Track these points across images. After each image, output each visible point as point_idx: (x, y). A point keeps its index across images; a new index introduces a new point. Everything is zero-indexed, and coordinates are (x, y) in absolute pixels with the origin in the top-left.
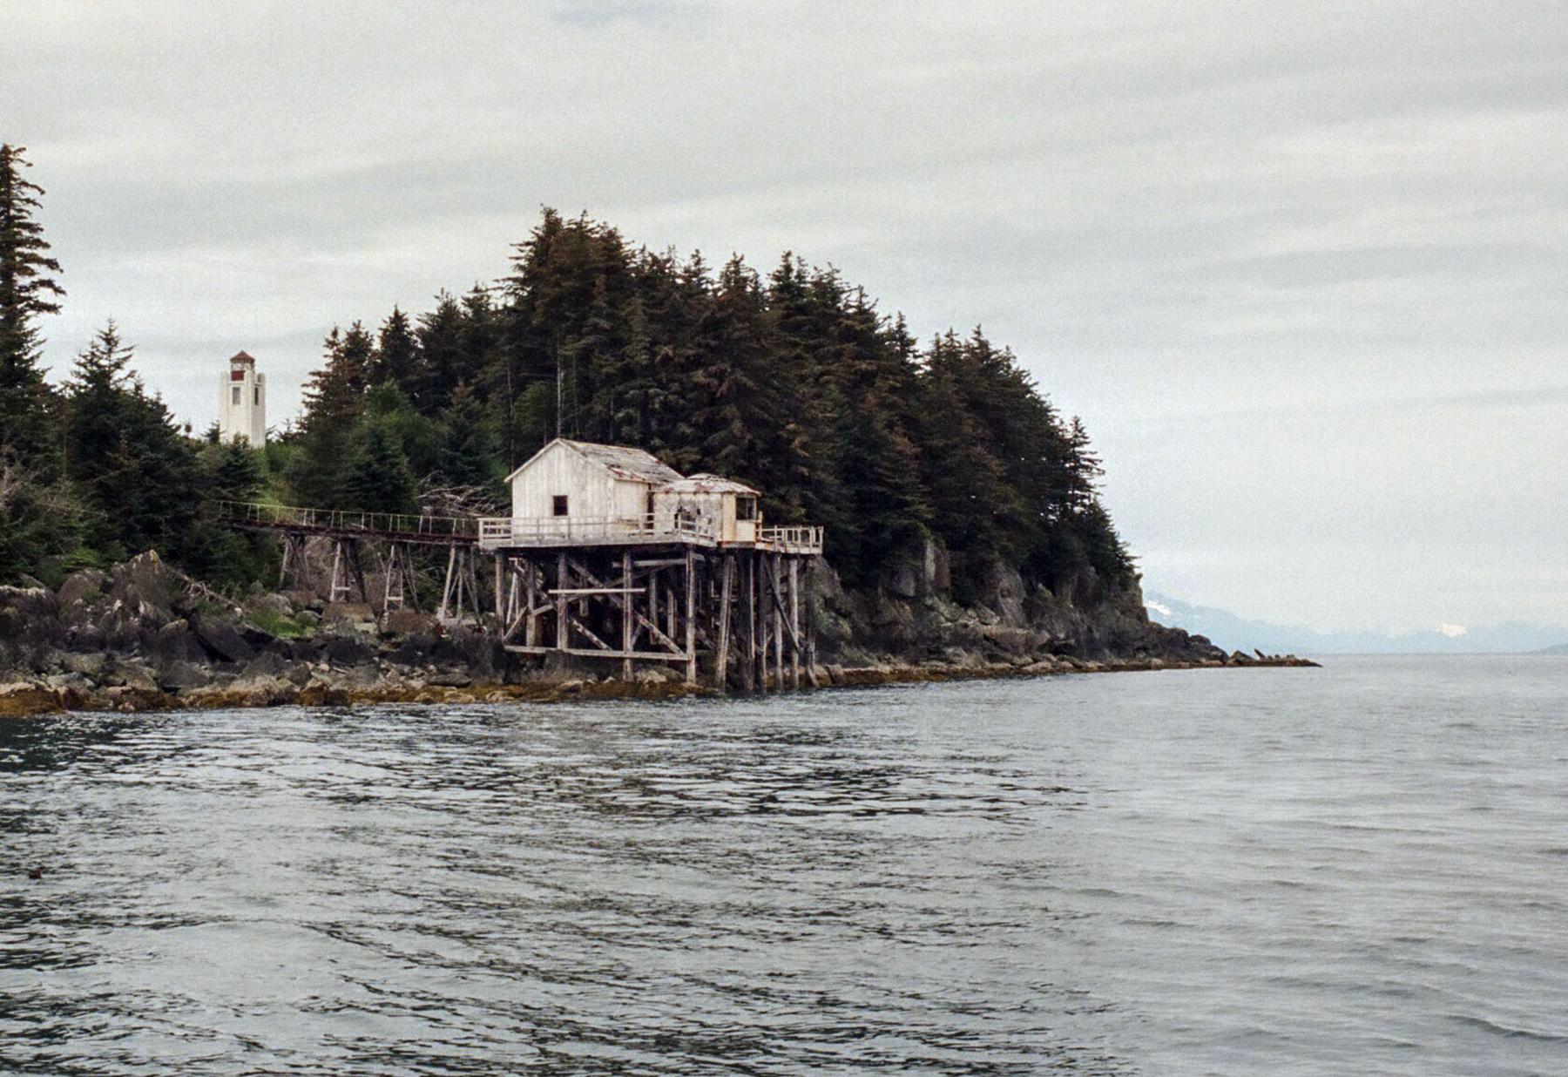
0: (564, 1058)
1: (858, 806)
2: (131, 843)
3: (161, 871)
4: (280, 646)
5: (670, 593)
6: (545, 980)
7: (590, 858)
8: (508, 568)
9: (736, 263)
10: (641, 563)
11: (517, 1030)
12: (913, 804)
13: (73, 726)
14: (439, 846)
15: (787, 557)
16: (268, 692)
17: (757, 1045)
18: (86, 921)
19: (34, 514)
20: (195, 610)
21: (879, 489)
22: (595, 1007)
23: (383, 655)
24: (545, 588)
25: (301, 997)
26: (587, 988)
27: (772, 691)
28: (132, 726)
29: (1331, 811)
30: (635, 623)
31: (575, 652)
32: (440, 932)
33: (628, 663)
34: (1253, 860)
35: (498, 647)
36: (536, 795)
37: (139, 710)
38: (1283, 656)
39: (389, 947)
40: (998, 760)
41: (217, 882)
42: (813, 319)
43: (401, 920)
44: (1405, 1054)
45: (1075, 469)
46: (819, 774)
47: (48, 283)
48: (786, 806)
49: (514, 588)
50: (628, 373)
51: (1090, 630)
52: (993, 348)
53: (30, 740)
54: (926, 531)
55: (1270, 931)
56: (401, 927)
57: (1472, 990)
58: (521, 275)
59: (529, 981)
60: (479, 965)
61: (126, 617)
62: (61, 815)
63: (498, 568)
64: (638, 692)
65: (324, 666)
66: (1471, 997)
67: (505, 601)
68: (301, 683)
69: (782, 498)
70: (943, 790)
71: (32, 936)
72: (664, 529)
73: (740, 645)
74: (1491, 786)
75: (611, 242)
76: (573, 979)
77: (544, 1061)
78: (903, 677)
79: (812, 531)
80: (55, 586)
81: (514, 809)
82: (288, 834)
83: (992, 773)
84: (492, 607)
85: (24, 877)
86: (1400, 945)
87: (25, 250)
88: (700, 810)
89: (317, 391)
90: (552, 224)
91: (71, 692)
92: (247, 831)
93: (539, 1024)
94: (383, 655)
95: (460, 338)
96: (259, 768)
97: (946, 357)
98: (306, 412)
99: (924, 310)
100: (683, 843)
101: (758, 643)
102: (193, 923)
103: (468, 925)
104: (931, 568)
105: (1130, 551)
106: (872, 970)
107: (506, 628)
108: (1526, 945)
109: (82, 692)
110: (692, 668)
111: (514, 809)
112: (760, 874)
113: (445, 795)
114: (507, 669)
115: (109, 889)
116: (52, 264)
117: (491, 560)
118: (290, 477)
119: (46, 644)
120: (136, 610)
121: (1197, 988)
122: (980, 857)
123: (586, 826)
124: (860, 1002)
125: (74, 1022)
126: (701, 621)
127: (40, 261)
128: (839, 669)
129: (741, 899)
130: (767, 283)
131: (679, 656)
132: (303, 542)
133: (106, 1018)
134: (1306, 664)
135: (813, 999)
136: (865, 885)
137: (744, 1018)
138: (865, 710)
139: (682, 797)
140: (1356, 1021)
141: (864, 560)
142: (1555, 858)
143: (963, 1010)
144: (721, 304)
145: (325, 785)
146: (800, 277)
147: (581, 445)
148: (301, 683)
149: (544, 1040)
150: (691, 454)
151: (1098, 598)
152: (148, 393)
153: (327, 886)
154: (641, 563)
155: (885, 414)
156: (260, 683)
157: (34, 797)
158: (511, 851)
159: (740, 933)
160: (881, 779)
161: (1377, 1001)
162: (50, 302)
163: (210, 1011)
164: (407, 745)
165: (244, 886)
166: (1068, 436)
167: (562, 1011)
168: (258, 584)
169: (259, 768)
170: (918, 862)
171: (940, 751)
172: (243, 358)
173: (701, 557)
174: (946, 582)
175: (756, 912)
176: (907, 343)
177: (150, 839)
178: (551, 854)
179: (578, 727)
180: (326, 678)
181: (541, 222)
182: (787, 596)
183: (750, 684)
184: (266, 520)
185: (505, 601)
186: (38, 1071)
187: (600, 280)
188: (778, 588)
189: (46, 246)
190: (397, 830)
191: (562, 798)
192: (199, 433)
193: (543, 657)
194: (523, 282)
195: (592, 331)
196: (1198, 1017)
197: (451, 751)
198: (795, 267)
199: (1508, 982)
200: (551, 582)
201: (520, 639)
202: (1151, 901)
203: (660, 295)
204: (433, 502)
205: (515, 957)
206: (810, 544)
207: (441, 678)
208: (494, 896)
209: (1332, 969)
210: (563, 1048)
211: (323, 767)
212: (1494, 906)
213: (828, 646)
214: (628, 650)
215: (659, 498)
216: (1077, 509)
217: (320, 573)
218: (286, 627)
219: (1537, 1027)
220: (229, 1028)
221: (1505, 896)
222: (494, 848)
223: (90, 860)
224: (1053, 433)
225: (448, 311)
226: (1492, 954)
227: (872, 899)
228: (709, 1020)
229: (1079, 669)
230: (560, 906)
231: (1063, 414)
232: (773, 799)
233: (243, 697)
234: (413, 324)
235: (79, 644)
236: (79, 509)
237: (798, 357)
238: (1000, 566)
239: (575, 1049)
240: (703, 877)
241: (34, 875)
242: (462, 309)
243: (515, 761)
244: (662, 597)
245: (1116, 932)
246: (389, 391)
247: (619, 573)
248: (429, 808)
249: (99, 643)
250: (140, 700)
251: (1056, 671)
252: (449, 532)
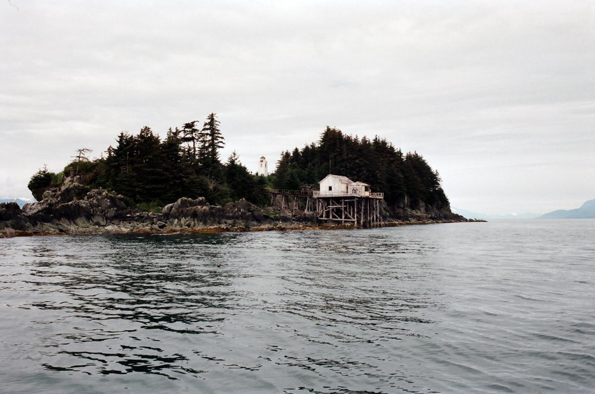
0: (332, 305)
1: (390, 251)
2: (239, 260)
3: (246, 266)
4: (271, 218)
5: (351, 207)
6: (328, 288)
7: (336, 263)
8: (319, 201)
9: (365, 137)
10: (346, 200)
11: (321, 299)
12: (403, 251)
13: (227, 235)
14: (305, 260)
15: (376, 199)
16: (268, 228)
17: (370, 302)
18: (230, 276)
19: (219, 190)
20: (253, 211)
21: (395, 185)
22: (337, 294)
23: (293, 220)
24: (327, 206)
25: (276, 292)
26: (336, 290)
27: (373, 227)
28: (240, 235)
29: (490, 252)
30: (344, 213)
31: (333, 219)
32: (306, 278)
33: (343, 222)
34: (474, 263)
35: (317, 218)
36: (325, 249)
37: (241, 232)
38: (480, 220)
39: (295, 281)
40: (420, 242)
41: (258, 268)
42: (381, 149)
43: (298, 275)
44: (505, 303)
45: (436, 180)
46: (383, 245)
47: (222, 142)
48: (377, 252)
49: (320, 206)
50: (343, 160)
51: (440, 214)
52: (418, 155)
53: (218, 238)
54: (405, 194)
55: (478, 278)
56: (298, 277)
57: (518, 290)
58: (322, 140)
59: (324, 288)
60: (314, 285)
61: (238, 212)
62: (225, 254)
63: (317, 201)
64: (345, 228)
65: (281, 222)
66: (518, 291)
67: (319, 209)
68: (276, 226)
69: (375, 187)
70: (408, 248)
71: (218, 279)
72: (350, 193)
73: (366, 218)
74: (523, 247)
75: (340, 133)
76: (333, 288)
77: (327, 305)
78: (401, 224)
79: (381, 194)
80: (223, 206)
81: (320, 252)
82: (273, 258)
83: (418, 244)
84: (316, 210)
85: (216, 267)
86: (504, 280)
87: (216, 135)
88: (357, 252)
89: (279, 164)
90: (329, 129)
91: (227, 228)
92: (264, 257)
93: (326, 297)
94: (293, 220)
95: (310, 152)
96: (266, 244)
97: (409, 157)
98: (276, 169)
99: (404, 147)
100: (354, 259)
101: (370, 217)
102: (253, 276)
103: (311, 277)
104: (406, 201)
105: (448, 198)
106: (394, 286)
107: (319, 214)
108: (530, 280)
109: (229, 228)
110: (356, 222)
111: (320, 252)
112: (371, 266)
113: (307, 249)
114: (319, 223)
115: (235, 269)
116: (222, 138)
117: (316, 200)
118: (273, 183)
119: (221, 218)
120: (240, 211)
121: (461, 290)
122: (416, 262)
123: (336, 256)
124: (391, 293)
125: (228, 297)
126: (358, 213)
127: (220, 137)
128: (387, 223)
129: (366, 271)
130: (372, 141)
131: (353, 220)
132: (276, 196)
133: (234, 296)
134: (485, 221)
135: (382, 292)
136: (392, 268)
137: (367, 296)
138: (392, 231)
139: (354, 250)
140: (496, 296)
141: (392, 200)
142: (536, 262)
143: (413, 294)
144: (361, 146)
145: (281, 247)
146: (379, 140)
147: (334, 176)
148: (276, 226)
149: (327, 301)
150: (356, 178)
151: (441, 208)
152: (243, 165)
153: (281, 268)
154: (346, 200)
155: (397, 169)
156: (266, 226)
157: (218, 250)
158: (320, 261)
159: (366, 278)
160: (396, 246)
161: (499, 292)
162: (222, 146)
163: (257, 295)
164: (299, 239)
165: (263, 268)
166: (435, 173)
167: (331, 295)
168: (266, 205)
169: (266, 244)
170: (404, 263)
171: (408, 240)
172: (263, 158)
173: (357, 199)
174: (409, 204)
175: (370, 274)
176: (401, 154)
177: (243, 259)
178: (329, 262)
179: (334, 235)
180: (281, 225)
181: (326, 129)
182: (376, 207)
183: (368, 226)
184: (268, 191)
185: (319, 209)
186: (219, 308)
187: (338, 141)
188: (375, 206)
189: (221, 134)
190: (297, 257)
191: (331, 250)
192: (254, 173)
193: (327, 220)
194: (322, 141)
195: (335, 152)
196: (460, 296)
197: (308, 240)
198: (378, 138)
199: (527, 288)
200: (329, 204)
201: (322, 216)
202: (452, 271)
203: (349, 144)
204: (304, 188)
205: (321, 283)
206: (381, 196)
207: (306, 225)
208: (316, 270)
209: (490, 285)
210: (331, 302)
211: (280, 244)
212: (524, 272)
213: (385, 218)
214: (343, 219)
215: (349, 187)
216: (437, 189)
217: (280, 203)
218: (272, 214)
219: (533, 298)
220: (261, 298)
221: (526, 270)
222: (317, 260)
223: (231, 263)
224: (432, 173)
225: (307, 148)
226: (523, 282)
227: (394, 271)
228: (359, 296)
229: (437, 222)
230: (330, 273)
231: (434, 169)
232: (374, 250)
233: (263, 229)
234: (300, 150)
235: (229, 218)
236: (228, 189)
237: (379, 157)
238: (420, 201)
239: (334, 303)
240: (358, 266)
241: (219, 266)
242: (310, 147)
243: (321, 242)
244: (350, 208)
245: (445, 278)
246: (295, 164)
247: (341, 203)
248: (303, 252)
249: (232, 218)
250: (241, 230)
251: (432, 223)
252: (307, 194)
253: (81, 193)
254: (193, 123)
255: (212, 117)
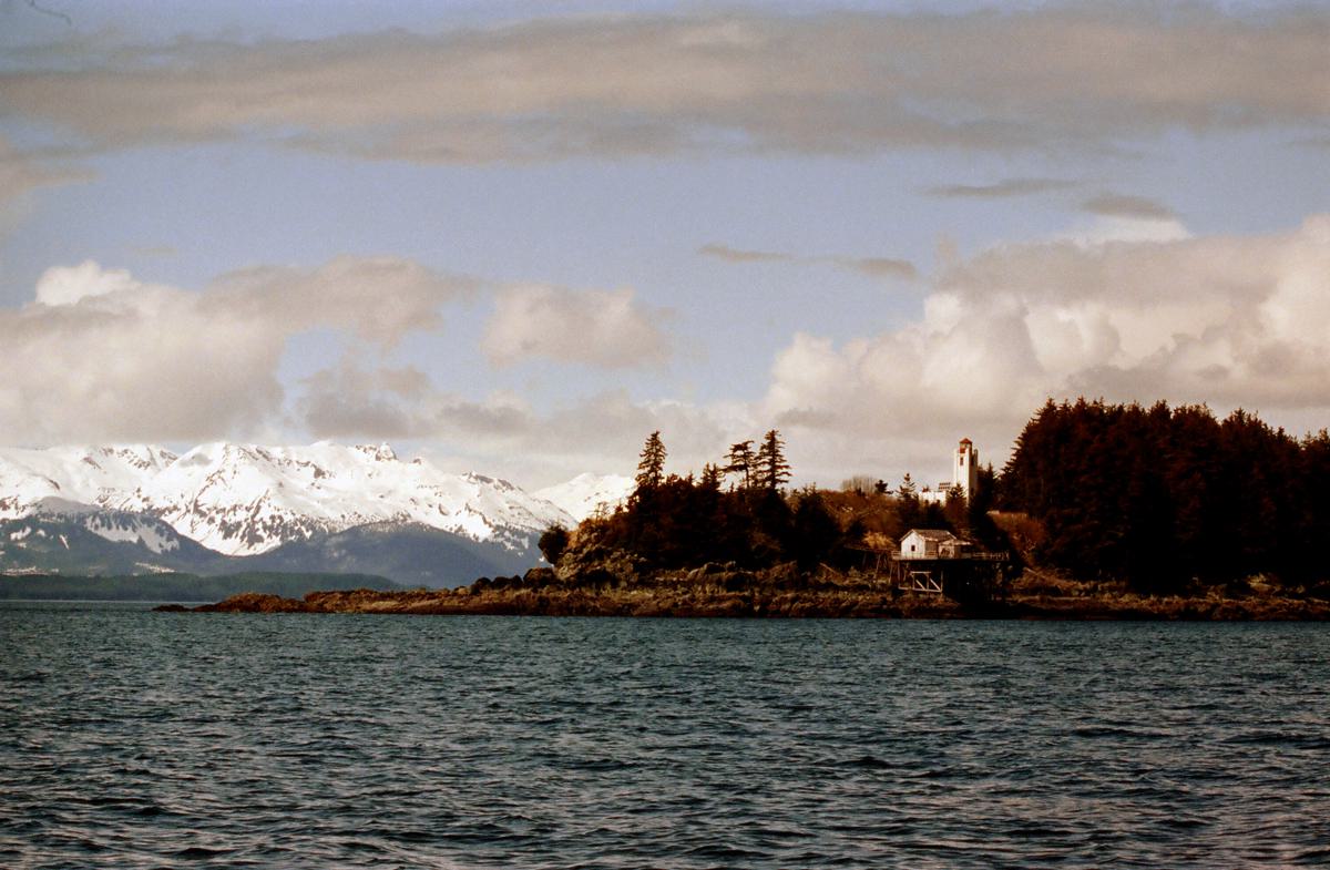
116: (787, 467)
172: (967, 442)
253: (600, 555)
254: (746, 443)
255: (772, 436)
